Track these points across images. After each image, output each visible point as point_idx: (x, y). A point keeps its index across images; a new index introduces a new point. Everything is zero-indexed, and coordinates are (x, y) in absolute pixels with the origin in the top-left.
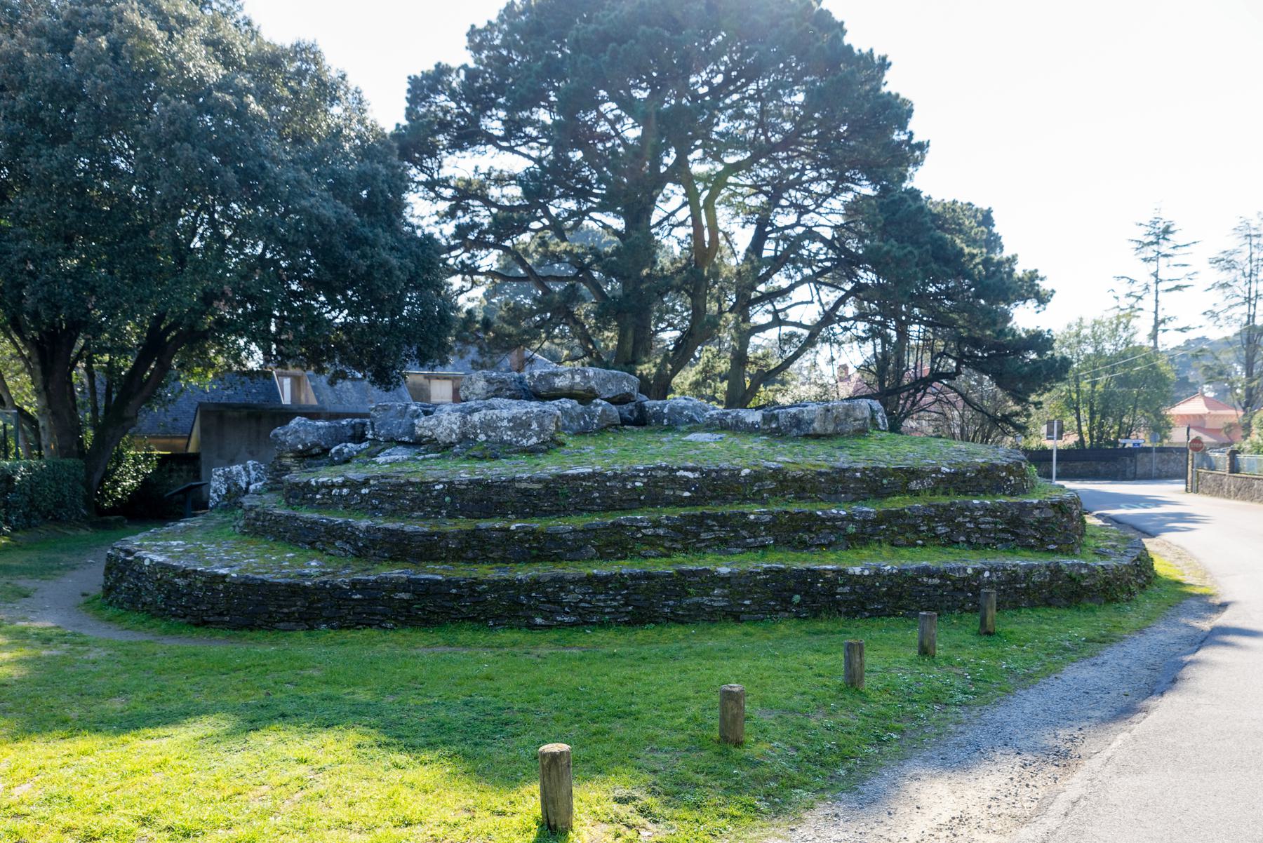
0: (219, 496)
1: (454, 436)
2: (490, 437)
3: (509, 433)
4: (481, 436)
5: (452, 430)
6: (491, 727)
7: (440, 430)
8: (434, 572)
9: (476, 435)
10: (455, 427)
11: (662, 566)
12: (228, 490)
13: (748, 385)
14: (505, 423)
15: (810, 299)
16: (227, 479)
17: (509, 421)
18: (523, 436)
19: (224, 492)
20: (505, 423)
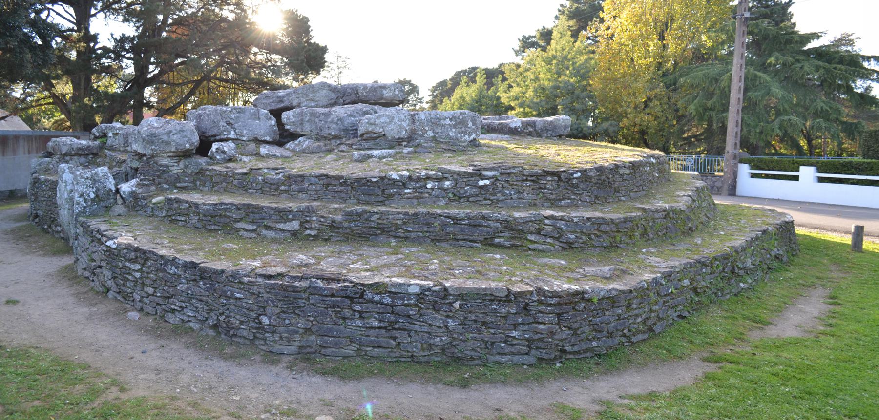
0: (85, 200)
1: (404, 132)
2: (437, 133)
3: (454, 130)
4: (428, 133)
5: (401, 127)
6: (153, 376)
7: (392, 126)
8: (613, 145)
9: (425, 132)
10: (405, 124)
11: (622, 157)
12: (96, 193)
13: (40, 42)
14: (448, 122)
15: (738, 192)
16: (95, 181)
17: (451, 120)
18: (465, 133)
19: (92, 196)
20: (448, 122)
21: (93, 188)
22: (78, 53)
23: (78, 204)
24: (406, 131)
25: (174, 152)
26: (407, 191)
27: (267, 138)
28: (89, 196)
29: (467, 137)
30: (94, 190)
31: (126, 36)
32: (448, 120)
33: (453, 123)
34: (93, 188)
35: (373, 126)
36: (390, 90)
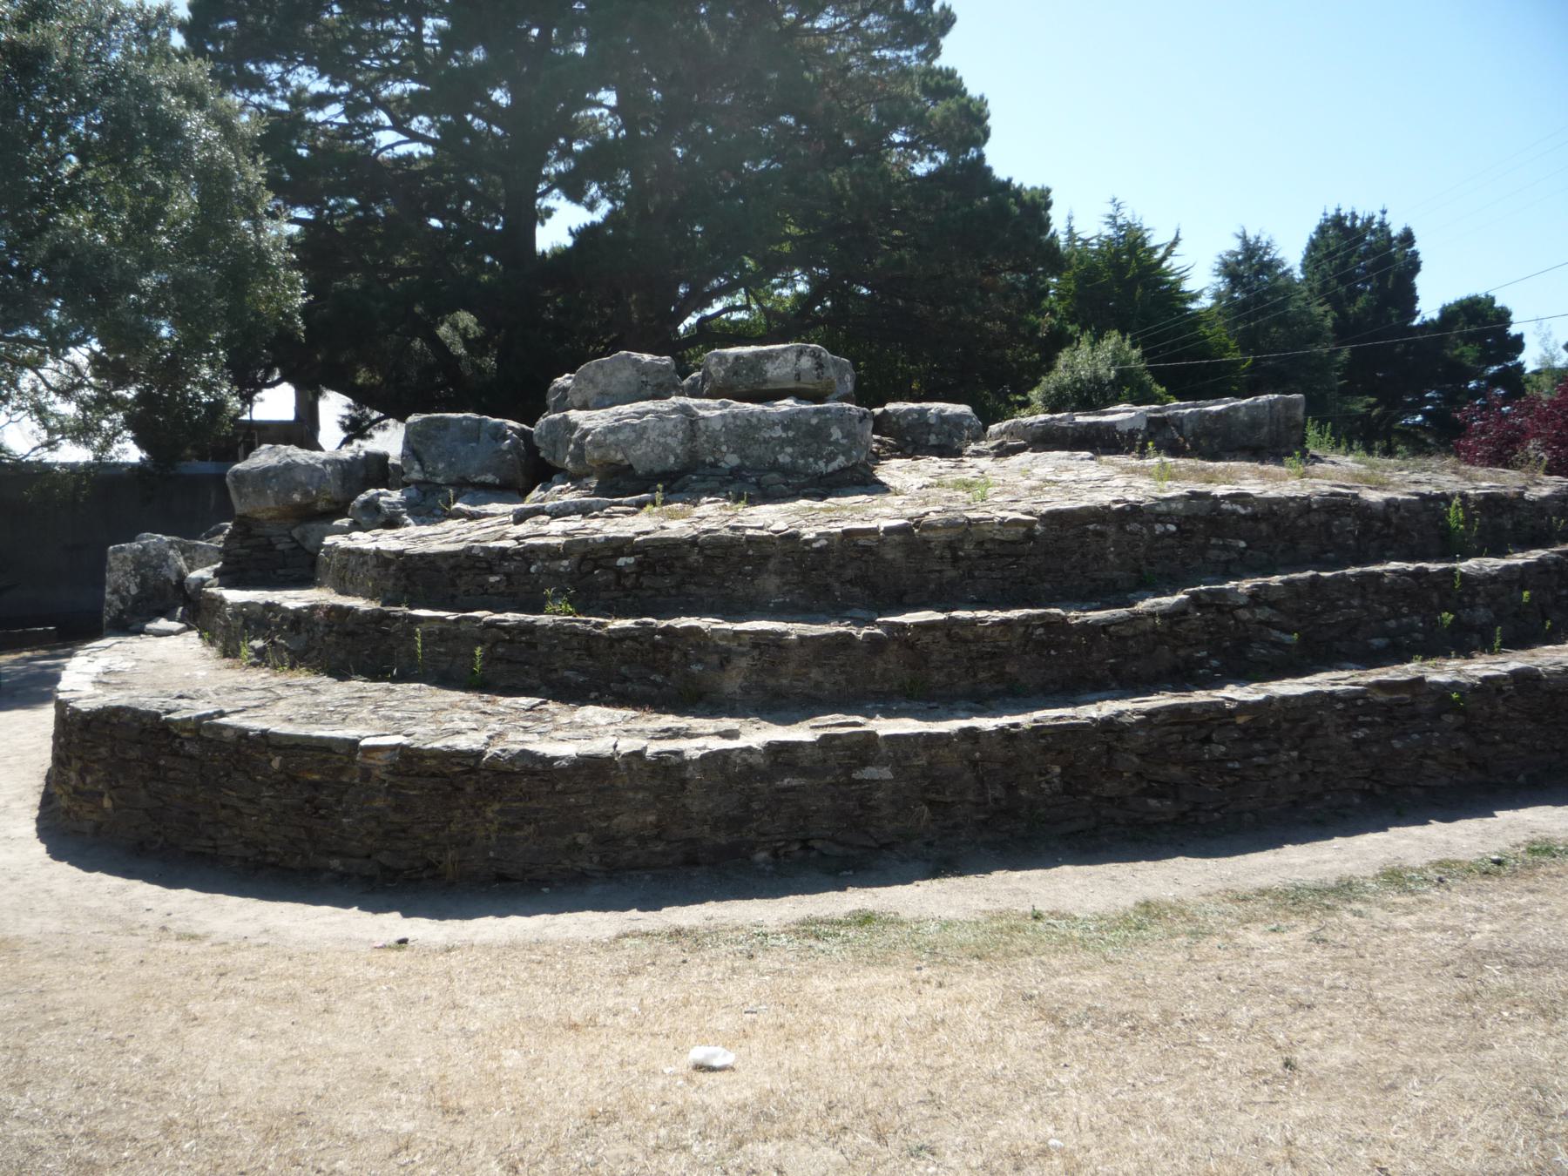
0: (123, 600)
1: (672, 460)
5: (666, 447)
17: (786, 428)
19: (134, 590)
20: (778, 432)
21: (135, 576)
22: (20, 265)
23: (110, 605)
24: (677, 457)
25: (275, 509)
26: (493, 579)
27: (489, 478)
28: (128, 592)
29: (821, 463)
30: (138, 580)
31: (1498, 304)
32: (778, 428)
33: (791, 434)
34: (135, 576)
35: (603, 450)
36: (786, 360)
